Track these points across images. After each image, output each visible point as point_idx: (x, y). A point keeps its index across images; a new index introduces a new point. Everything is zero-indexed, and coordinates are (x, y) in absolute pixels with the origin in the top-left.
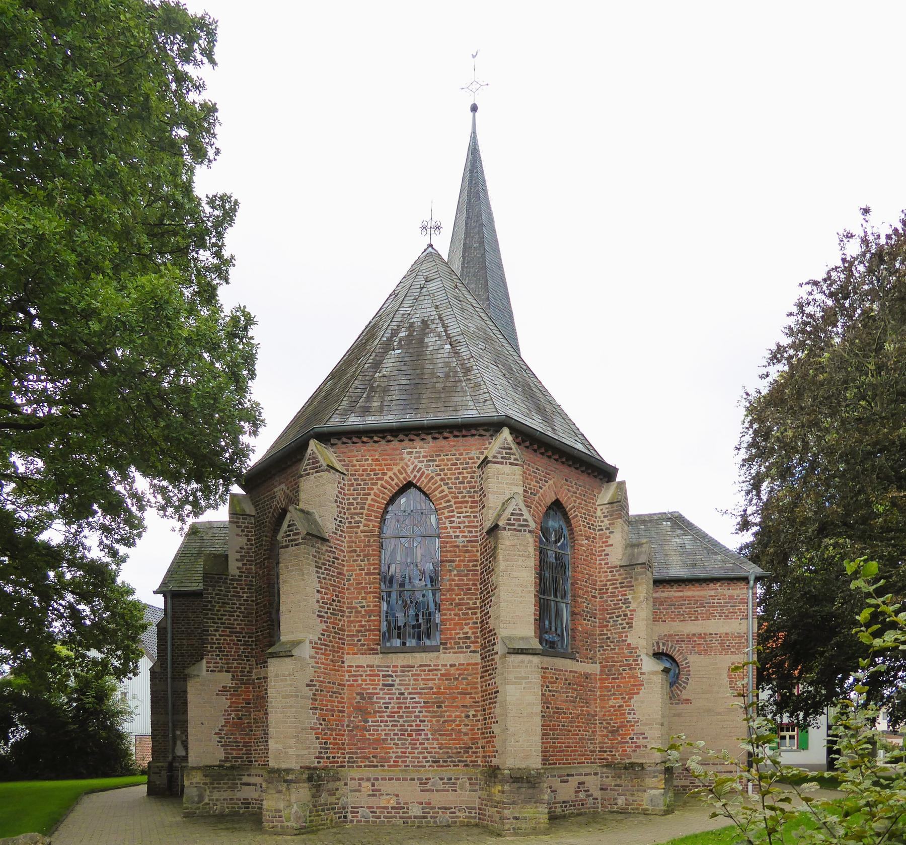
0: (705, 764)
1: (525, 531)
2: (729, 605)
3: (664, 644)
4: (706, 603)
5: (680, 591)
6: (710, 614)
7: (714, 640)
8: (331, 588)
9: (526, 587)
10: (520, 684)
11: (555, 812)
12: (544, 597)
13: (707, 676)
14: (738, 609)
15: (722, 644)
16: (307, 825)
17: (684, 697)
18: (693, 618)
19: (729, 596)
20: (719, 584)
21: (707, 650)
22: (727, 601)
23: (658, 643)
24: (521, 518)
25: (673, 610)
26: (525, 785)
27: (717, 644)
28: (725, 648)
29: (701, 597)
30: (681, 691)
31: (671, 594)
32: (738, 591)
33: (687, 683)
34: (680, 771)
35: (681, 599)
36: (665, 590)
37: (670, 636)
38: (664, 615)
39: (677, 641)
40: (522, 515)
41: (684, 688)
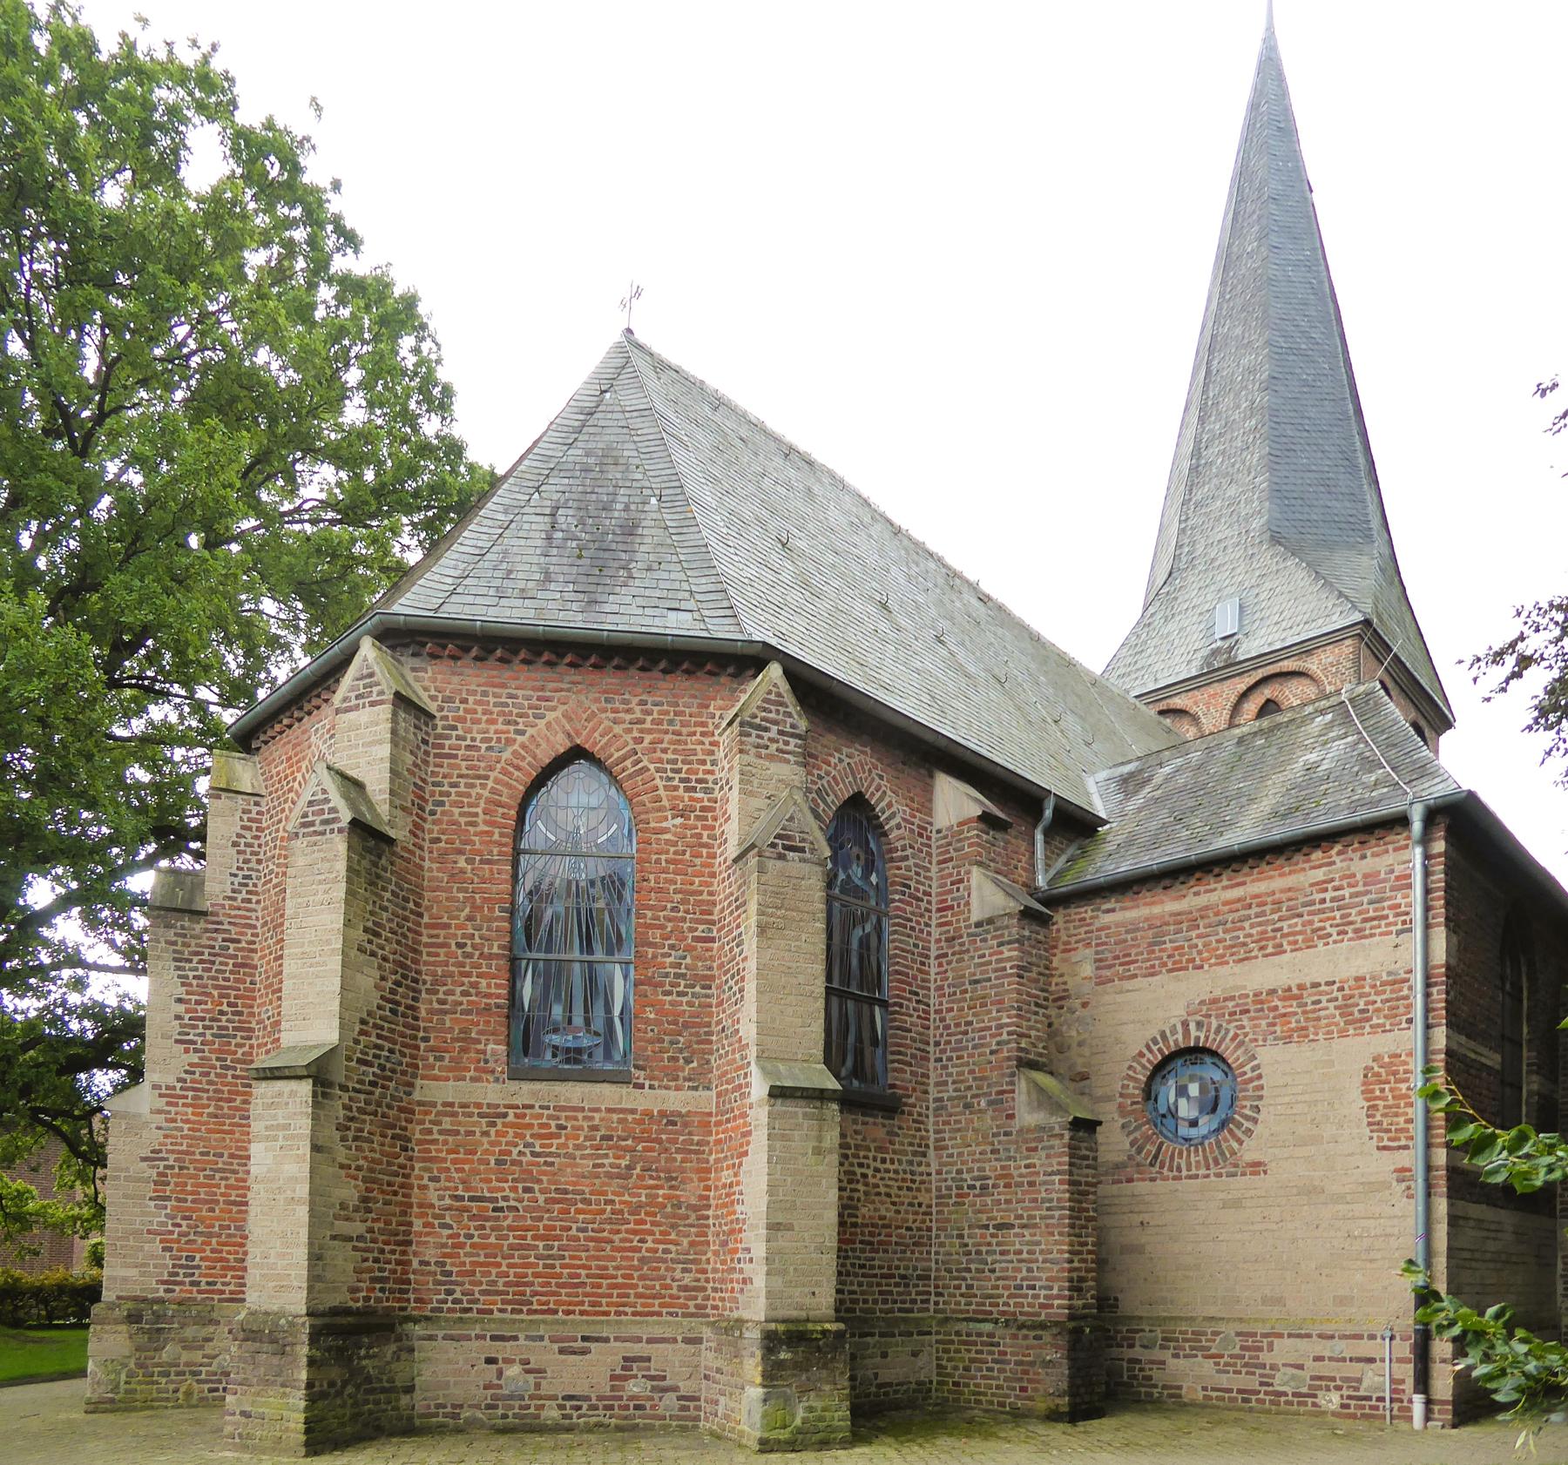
0: (1299, 1336)
1: (332, 831)
2: (1365, 899)
3: (1199, 1025)
4: (1305, 905)
5: (1239, 885)
6: (1314, 931)
7: (1324, 999)
8: (215, 993)
9: (328, 942)
10: (275, 1139)
11: (537, 1417)
12: (550, 956)
13: (1307, 1097)
14: (1390, 908)
15: (1345, 1010)
16: (117, 1397)
17: (1249, 1157)
18: (1270, 950)
19: (1366, 876)
20: (1338, 847)
21: (1305, 1028)
22: (1360, 888)
23: (1185, 1024)
24: (326, 807)
25: (1221, 935)
26: (266, 1347)
27: (1332, 1010)
28: (1355, 1019)
29: (1290, 890)
30: (1241, 1142)
31: (1213, 898)
32: (1382, 860)
33: (1255, 1121)
34: (1237, 1351)
35: (1239, 905)
36: (1202, 889)
37: (1214, 1001)
38: (1200, 953)
39: (1231, 1014)
40: (327, 801)
41: (1249, 1132)
